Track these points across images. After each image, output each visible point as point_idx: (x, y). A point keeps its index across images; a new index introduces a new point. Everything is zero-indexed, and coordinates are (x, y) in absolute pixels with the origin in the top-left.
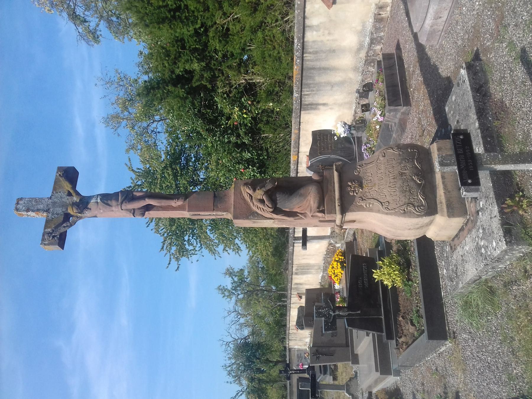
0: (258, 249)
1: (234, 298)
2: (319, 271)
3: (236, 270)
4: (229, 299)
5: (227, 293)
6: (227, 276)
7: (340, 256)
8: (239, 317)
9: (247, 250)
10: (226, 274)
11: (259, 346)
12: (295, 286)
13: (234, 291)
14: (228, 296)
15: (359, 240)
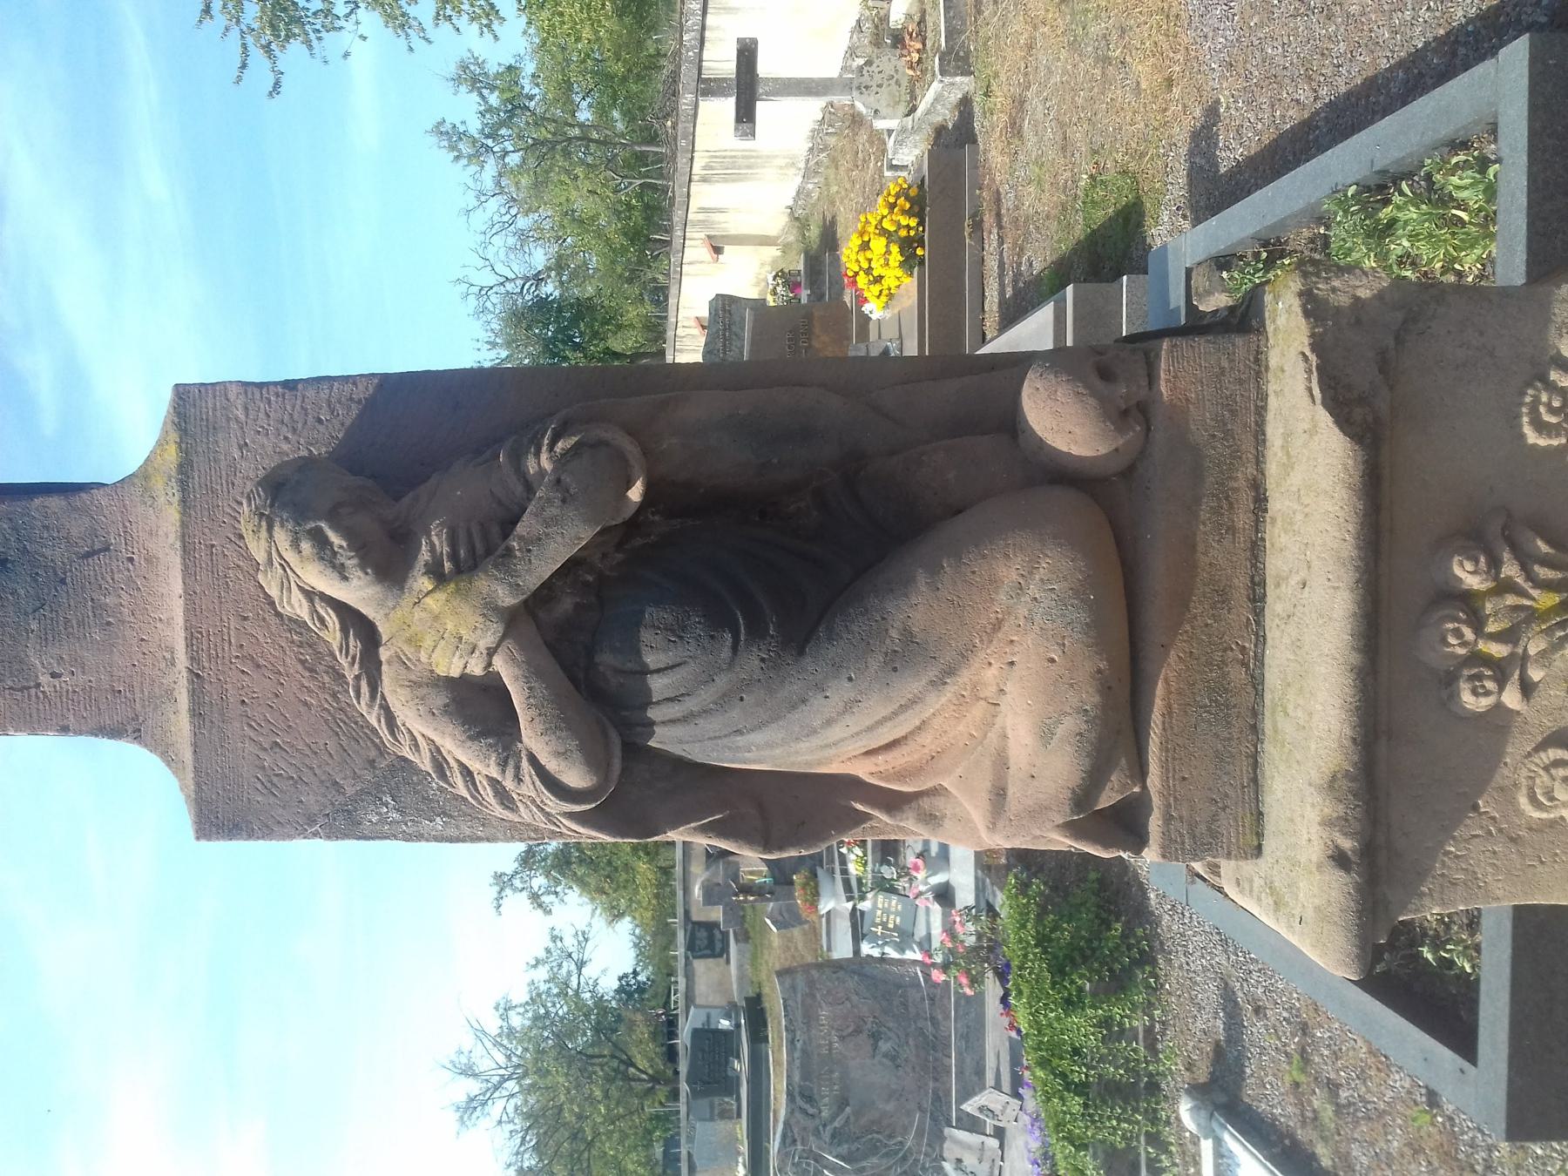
0: (561, 14)
1: (491, 168)
2: (793, 171)
3: (492, 68)
4: (474, 168)
5: (465, 148)
6: (463, 89)
7: (904, 212)
8: (514, 211)
9: (524, 19)
10: (458, 80)
11: (583, 310)
12: (701, 217)
13: (490, 142)
14: (470, 157)
15: (993, 151)
